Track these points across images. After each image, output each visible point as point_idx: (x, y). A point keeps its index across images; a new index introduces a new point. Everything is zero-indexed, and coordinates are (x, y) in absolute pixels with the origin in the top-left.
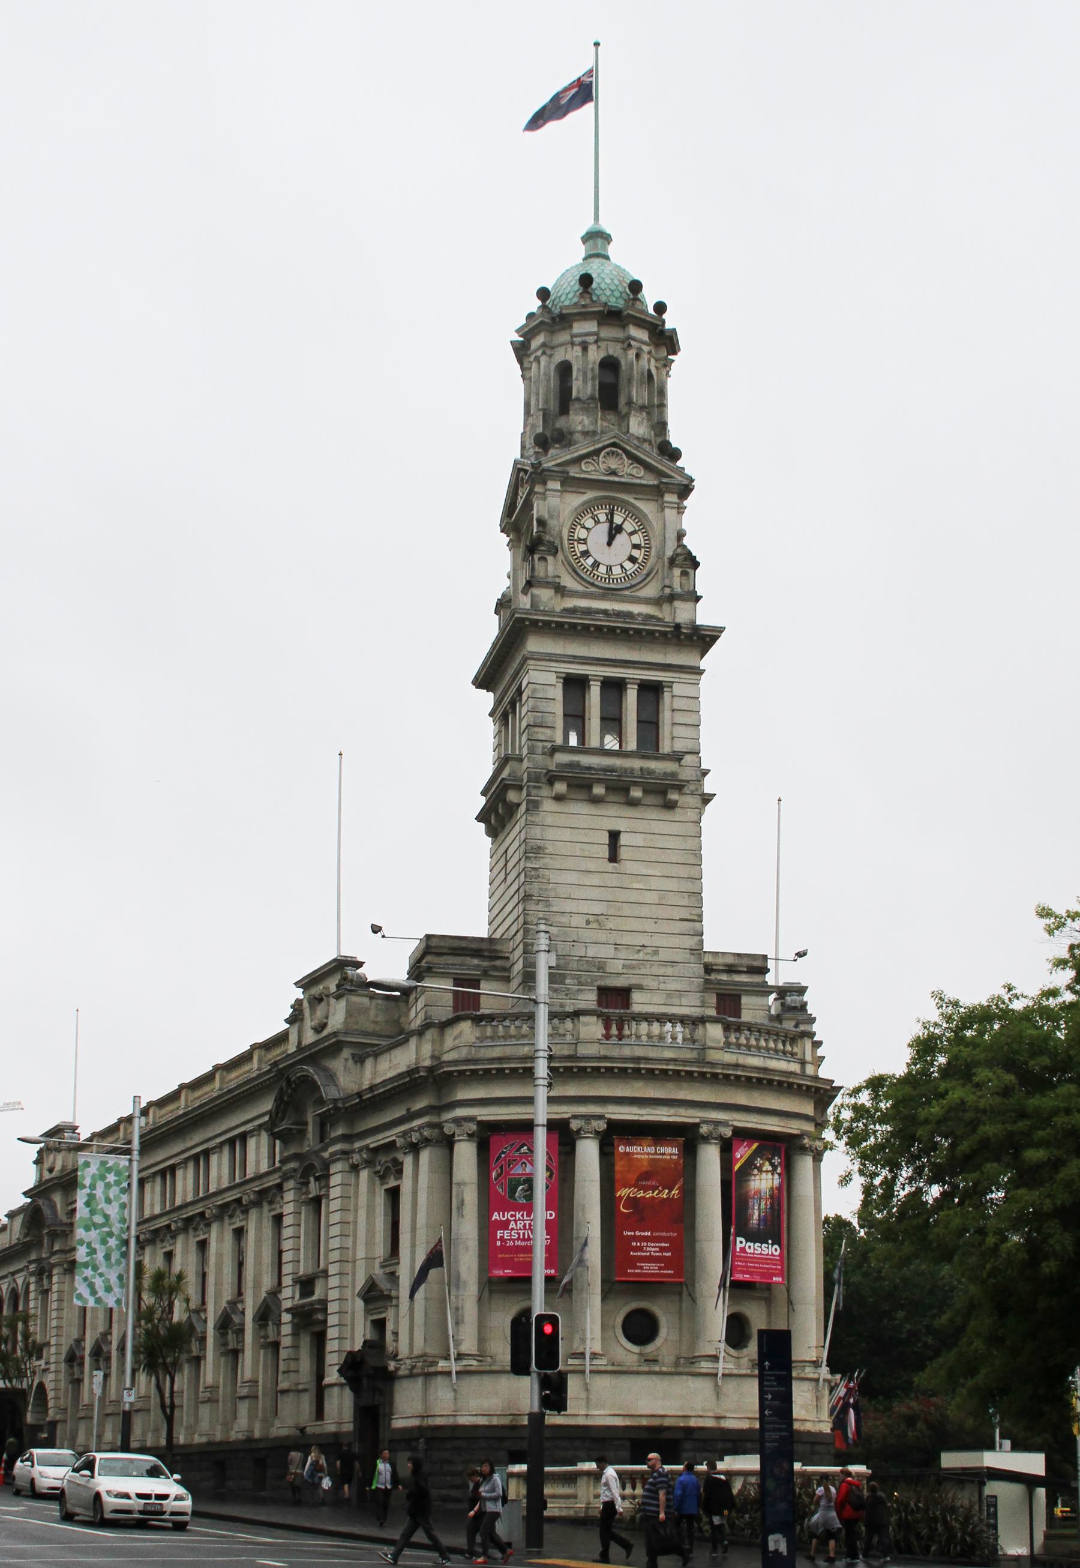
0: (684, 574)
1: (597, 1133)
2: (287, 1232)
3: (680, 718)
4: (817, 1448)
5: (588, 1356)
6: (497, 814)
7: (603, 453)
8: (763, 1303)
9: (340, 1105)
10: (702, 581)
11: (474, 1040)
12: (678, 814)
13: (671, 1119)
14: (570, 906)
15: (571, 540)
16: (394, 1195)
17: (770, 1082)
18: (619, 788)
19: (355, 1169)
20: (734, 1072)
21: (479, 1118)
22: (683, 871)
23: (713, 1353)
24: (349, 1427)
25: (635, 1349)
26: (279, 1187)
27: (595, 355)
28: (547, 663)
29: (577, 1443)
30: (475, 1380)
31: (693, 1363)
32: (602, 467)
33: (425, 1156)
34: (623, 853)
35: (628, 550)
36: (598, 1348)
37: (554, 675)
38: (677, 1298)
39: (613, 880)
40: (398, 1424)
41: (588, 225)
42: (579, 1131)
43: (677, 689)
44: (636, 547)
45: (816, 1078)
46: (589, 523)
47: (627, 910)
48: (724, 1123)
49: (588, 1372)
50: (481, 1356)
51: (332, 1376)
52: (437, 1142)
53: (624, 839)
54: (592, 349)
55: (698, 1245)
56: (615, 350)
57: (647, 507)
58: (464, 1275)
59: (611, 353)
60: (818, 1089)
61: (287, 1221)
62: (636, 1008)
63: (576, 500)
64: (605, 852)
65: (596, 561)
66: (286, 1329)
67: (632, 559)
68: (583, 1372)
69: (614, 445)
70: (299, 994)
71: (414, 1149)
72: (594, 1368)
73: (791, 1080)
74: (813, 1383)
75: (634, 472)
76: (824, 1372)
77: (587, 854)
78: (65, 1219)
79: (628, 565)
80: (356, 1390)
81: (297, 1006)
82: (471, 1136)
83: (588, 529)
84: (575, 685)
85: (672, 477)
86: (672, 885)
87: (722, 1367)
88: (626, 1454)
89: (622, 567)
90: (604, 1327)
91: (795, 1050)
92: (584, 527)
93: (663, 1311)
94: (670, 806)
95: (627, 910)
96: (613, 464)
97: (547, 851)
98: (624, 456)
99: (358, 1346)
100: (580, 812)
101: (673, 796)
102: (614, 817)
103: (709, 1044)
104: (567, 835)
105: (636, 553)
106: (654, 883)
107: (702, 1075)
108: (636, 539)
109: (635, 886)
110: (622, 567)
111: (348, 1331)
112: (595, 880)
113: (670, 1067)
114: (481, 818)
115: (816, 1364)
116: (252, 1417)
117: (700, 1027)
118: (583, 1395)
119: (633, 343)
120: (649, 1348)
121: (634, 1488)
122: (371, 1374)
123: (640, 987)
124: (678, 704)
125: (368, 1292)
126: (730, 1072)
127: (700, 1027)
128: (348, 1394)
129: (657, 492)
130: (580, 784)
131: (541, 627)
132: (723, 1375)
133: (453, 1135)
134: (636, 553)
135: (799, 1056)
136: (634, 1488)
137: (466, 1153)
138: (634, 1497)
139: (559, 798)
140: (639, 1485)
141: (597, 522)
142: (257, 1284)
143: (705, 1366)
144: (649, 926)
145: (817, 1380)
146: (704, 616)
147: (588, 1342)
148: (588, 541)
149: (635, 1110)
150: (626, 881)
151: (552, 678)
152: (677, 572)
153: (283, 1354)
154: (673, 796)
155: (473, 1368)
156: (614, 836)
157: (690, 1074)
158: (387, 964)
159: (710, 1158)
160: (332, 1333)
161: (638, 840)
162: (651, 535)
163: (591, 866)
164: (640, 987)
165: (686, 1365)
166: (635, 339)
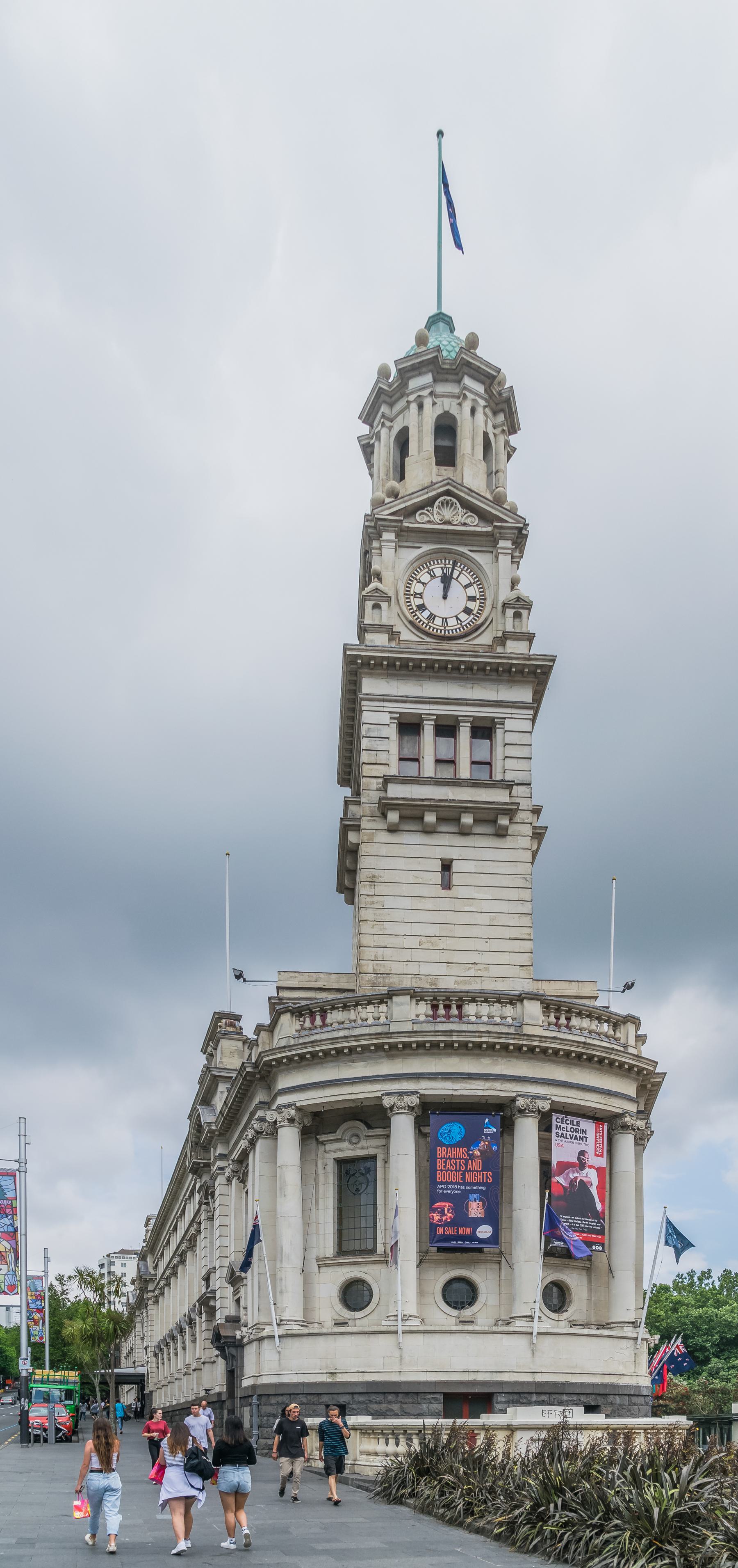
0: (517, 615)
1: (411, 1108)
3: (511, 751)
4: (635, 1400)
5: (400, 1318)
7: (437, 503)
8: (584, 1272)
9: (214, 1128)
10: (532, 623)
11: (294, 1032)
12: (508, 842)
13: (487, 1093)
15: (407, 594)
17: (590, 1058)
18: (450, 816)
19: (229, 1180)
20: (553, 1046)
21: (298, 1104)
23: (529, 1314)
25: (455, 1313)
27: (430, 414)
28: (382, 704)
29: (390, 1397)
30: (296, 1343)
31: (508, 1323)
32: (437, 518)
34: (456, 879)
35: (463, 603)
36: (412, 1310)
37: (388, 715)
38: (496, 1266)
39: (445, 904)
42: (391, 1108)
43: (509, 724)
44: (472, 599)
45: (638, 1057)
46: (425, 578)
47: (459, 931)
48: (544, 1098)
49: (400, 1332)
50: (305, 1323)
52: (268, 1134)
53: (455, 867)
54: (428, 402)
55: (514, 1213)
56: (449, 405)
57: (482, 559)
58: (287, 1248)
60: (640, 1071)
63: (410, 555)
64: (437, 878)
65: (431, 614)
67: (467, 611)
68: (396, 1332)
69: (448, 493)
72: (407, 1328)
73: (612, 1057)
74: (631, 1342)
75: (468, 521)
76: (643, 1332)
77: (420, 881)
78: (153, 1272)
79: (463, 617)
80: (224, 1357)
82: (291, 1120)
83: (423, 584)
84: (409, 727)
85: (507, 522)
86: (504, 907)
87: (536, 1326)
88: (440, 1407)
89: (457, 618)
90: (421, 1293)
91: (618, 1035)
92: (420, 582)
93: (482, 1277)
94: (501, 833)
95: (459, 931)
96: (447, 514)
97: (381, 879)
100: (413, 842)
101: (504, 821)
103: (526, 1021)
104: (400, 864)
105: (471, 605)
106: (486, 906)
107: (519, 1048)
108: (471, 591)
109: (466, 909)
110: (457, 618)
112: (429, 904)
113: (483, 1040)
115: (635, 1324)
117: (518, 1005)
118: (397, 1353)
119: (467, 394)
120: (467, 1313)
121: (397, 1444)
124: (510, 738)
125: (231, 1278)
126: (548, 1045)
127: (518, 1005)
129: (489, 542)
130: (412, 816)
131: (512, 1051)
132: (538, 1333)
133: (275, 1122)
134: (471, 605)
135: (622, 1041)
136: (397, 1444)
138: (397, 1455)
139: (392, 830)
140: (402, 1442)
141: (433, 577)
143: (520, 1325)
144: (480, 945)
145: (636, 1339)
147: (400, 1303)
148: (424, 595)
149: (449, 1084)
150: (457, 905)
151: (385, 718)
152: (510, 612)
154: (504, 821)
155: (294, 1332)
156: (446, 866)
157: (505, 1047)
159: (527, 1130)
162: (486, 586)
163: (425, 891)
165: (504, 1324)
166: (470, 391)
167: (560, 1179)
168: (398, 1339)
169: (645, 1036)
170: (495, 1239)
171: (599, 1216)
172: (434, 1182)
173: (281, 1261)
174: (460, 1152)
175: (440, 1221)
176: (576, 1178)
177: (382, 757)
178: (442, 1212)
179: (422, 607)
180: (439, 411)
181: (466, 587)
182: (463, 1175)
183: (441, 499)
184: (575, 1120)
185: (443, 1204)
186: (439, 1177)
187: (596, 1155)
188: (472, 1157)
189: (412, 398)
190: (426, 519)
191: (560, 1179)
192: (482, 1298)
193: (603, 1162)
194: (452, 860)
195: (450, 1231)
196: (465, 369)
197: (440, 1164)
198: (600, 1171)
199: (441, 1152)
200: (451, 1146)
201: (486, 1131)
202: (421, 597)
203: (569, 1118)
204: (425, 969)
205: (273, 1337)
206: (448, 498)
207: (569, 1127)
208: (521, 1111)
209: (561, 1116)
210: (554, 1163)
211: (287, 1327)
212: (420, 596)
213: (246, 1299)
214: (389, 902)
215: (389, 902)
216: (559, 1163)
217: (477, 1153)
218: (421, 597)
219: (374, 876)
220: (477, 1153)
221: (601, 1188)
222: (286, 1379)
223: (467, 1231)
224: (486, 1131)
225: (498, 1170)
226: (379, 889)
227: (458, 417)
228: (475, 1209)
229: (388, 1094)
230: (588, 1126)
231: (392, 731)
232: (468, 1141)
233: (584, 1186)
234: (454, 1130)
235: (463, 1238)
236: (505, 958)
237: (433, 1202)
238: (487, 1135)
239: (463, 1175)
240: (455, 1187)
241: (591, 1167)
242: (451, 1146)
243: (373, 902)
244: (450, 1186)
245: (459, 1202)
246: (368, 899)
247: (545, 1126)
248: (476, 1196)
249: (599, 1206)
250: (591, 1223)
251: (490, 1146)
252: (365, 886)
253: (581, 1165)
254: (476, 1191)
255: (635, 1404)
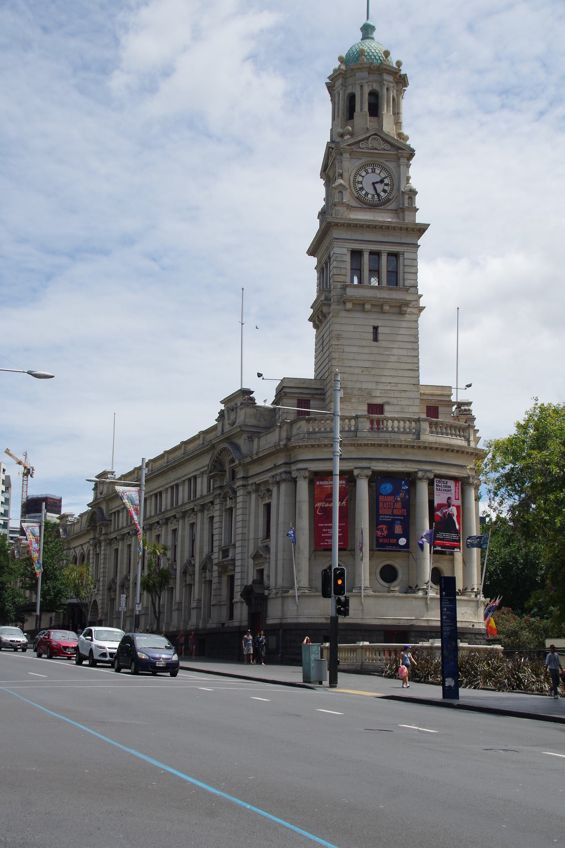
1: (367, 476)
2: (216, 525)
6: (319, 317)
7: (370, 139)
14: (353, 364)
15: (354, 181)
16: (268, 507)
22: (410, 346)
24: (245, 623)
26: (212, 503)
33: (283, 487)
34: (380, 337)
37: (346, 250)
40: (270, 621)
41: (363, 21)
42: (357, 476)
46: (363, 174)
48: (430, 471)
51: (237, 597)
53: (380, 330)
56: (376, 86)
59: (374, 88)
61: (216, 519)
62: (387, 414)
64: (371, 336)
65: (366, 192)
66: (215, 574)
69: (375, 134)
70: (222, 407)
71: (278, 483)
72: (366, 594)
76: (481, 598)
77: (362, 337)
81: (222, 413)
82: (305, 478)
84: (356, 254)
86: (404, 352)
91: (465, 434)
97: (343, 336)
98: (381, 140)
99: (250, 583)
102: (373, 320)
104: (352, 328)
111: (244, 575)
112: (367, 350)
114: (310, 320)
116: (198, 617)
118: (360, 608)
122: (256, 596)
123: (388, 403)
127: (418, 423)
128: (245, 607)
137: (303, 487)
142: (201, 552)
146: (420, 218)
151: (345, 251)
153: (214, 586)
156: (376, 328)
158: (265, 396)
159: (423, 488)
160: (237, 576)
161: (387, 330)
163: (365, 343)
164: (388, 403)
167: (439, 513)
168: (361, 600)
169: (478, 430)
170: (407, 546)
171: (457, 532)
172: (378, 515)
173: (299, 554)
174: (390, 499)
175: (381, 535)
176: (446, 512)
177: (343, 272)
178: (382, 530)
179: (362, 189)
180: (370, 89)
181: (367, 173)
182: (392, 510)
183: (372, 137)
184: (445, 481)
185: (383, 526)
186: (381, 512)
187: (456, 499)
188: (397, 501)
189: (358, 82)
190: (365, 146)
191: (439, 513)
192: (400, 576)
193: (459, 503)
194: (378, 327)
195: (386, 541)
196: (384, 71)
197: (381, 505)
198: (458, 507)
199: (381, 498)
200: (386, 495)
201: (403, 488)
202: (362, 184)
203: (442, 480)
204: (364, 386)
205: (295, 596)
206: (376, 137)
207: (443, 485)
208: (420, 479)
209: (438, 479)
210: (436, 504)
211: (302, 591)
212: (361, 183)
213: (269, 570)
214: (347, 349)
215: (347, 349)
216: (438, 504)
217: (399, 499)
218: (362, 184)
219: (339, 335)
220: (399, 499)
221: (458, 517)
222: (302, 620)
223: (394, 541)
224: (403, 488)
225: (409, 505)
226: (342, 342)
227: (380, 92)
228: (398, 529)
229: (356, 468)
230: (451, 483)
231: (348, 258)
232: (394, 493)
233: (450, 516)
234: (388, 487)
235: (392, 545)
236: (406, 380)
237: (377, 525)
238: (403, 490)
239: (392, 510)
240: (388, 517)
241: (453, 506)
242: (386, 495)
243: (338, 349)
244: (386, 517)
245: (390, 525)
246: (336, 347)
247: (431, 483)
248: (398, 522)
249: (457, 527)
250: (454, 536)
251: (405, 496)
252: (334, 340)
253: (449, 505)
254: (398, 520)
255: (478, 639)
